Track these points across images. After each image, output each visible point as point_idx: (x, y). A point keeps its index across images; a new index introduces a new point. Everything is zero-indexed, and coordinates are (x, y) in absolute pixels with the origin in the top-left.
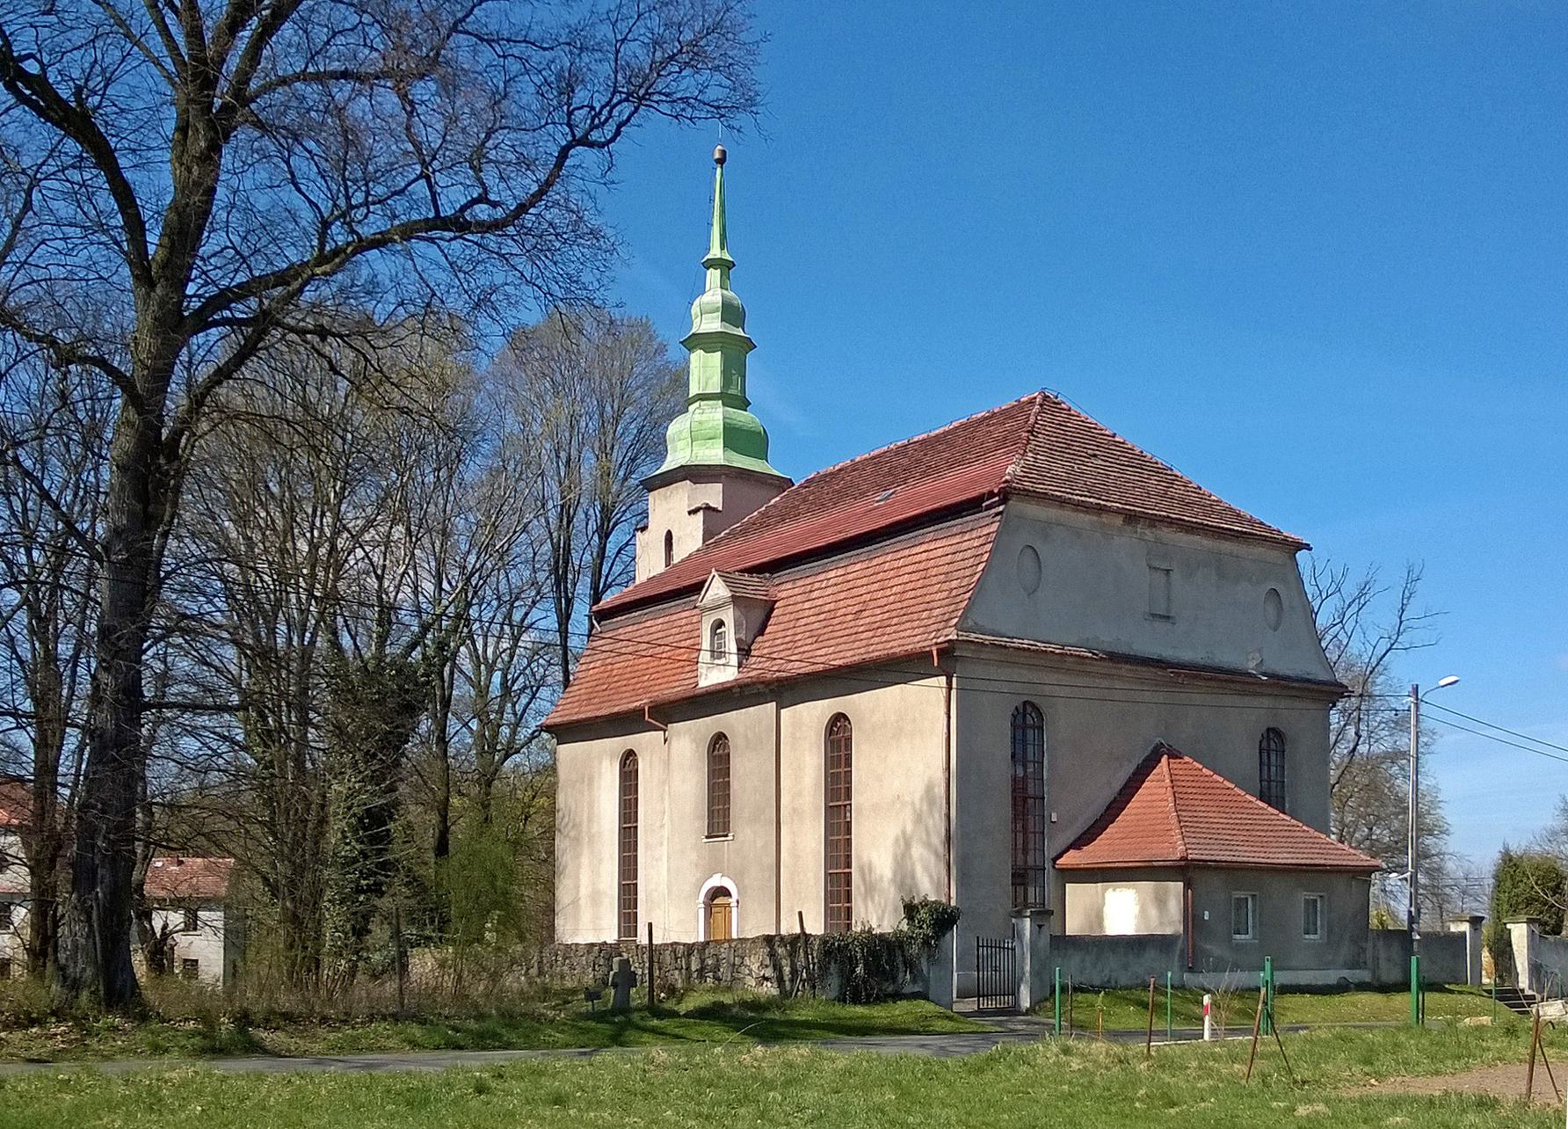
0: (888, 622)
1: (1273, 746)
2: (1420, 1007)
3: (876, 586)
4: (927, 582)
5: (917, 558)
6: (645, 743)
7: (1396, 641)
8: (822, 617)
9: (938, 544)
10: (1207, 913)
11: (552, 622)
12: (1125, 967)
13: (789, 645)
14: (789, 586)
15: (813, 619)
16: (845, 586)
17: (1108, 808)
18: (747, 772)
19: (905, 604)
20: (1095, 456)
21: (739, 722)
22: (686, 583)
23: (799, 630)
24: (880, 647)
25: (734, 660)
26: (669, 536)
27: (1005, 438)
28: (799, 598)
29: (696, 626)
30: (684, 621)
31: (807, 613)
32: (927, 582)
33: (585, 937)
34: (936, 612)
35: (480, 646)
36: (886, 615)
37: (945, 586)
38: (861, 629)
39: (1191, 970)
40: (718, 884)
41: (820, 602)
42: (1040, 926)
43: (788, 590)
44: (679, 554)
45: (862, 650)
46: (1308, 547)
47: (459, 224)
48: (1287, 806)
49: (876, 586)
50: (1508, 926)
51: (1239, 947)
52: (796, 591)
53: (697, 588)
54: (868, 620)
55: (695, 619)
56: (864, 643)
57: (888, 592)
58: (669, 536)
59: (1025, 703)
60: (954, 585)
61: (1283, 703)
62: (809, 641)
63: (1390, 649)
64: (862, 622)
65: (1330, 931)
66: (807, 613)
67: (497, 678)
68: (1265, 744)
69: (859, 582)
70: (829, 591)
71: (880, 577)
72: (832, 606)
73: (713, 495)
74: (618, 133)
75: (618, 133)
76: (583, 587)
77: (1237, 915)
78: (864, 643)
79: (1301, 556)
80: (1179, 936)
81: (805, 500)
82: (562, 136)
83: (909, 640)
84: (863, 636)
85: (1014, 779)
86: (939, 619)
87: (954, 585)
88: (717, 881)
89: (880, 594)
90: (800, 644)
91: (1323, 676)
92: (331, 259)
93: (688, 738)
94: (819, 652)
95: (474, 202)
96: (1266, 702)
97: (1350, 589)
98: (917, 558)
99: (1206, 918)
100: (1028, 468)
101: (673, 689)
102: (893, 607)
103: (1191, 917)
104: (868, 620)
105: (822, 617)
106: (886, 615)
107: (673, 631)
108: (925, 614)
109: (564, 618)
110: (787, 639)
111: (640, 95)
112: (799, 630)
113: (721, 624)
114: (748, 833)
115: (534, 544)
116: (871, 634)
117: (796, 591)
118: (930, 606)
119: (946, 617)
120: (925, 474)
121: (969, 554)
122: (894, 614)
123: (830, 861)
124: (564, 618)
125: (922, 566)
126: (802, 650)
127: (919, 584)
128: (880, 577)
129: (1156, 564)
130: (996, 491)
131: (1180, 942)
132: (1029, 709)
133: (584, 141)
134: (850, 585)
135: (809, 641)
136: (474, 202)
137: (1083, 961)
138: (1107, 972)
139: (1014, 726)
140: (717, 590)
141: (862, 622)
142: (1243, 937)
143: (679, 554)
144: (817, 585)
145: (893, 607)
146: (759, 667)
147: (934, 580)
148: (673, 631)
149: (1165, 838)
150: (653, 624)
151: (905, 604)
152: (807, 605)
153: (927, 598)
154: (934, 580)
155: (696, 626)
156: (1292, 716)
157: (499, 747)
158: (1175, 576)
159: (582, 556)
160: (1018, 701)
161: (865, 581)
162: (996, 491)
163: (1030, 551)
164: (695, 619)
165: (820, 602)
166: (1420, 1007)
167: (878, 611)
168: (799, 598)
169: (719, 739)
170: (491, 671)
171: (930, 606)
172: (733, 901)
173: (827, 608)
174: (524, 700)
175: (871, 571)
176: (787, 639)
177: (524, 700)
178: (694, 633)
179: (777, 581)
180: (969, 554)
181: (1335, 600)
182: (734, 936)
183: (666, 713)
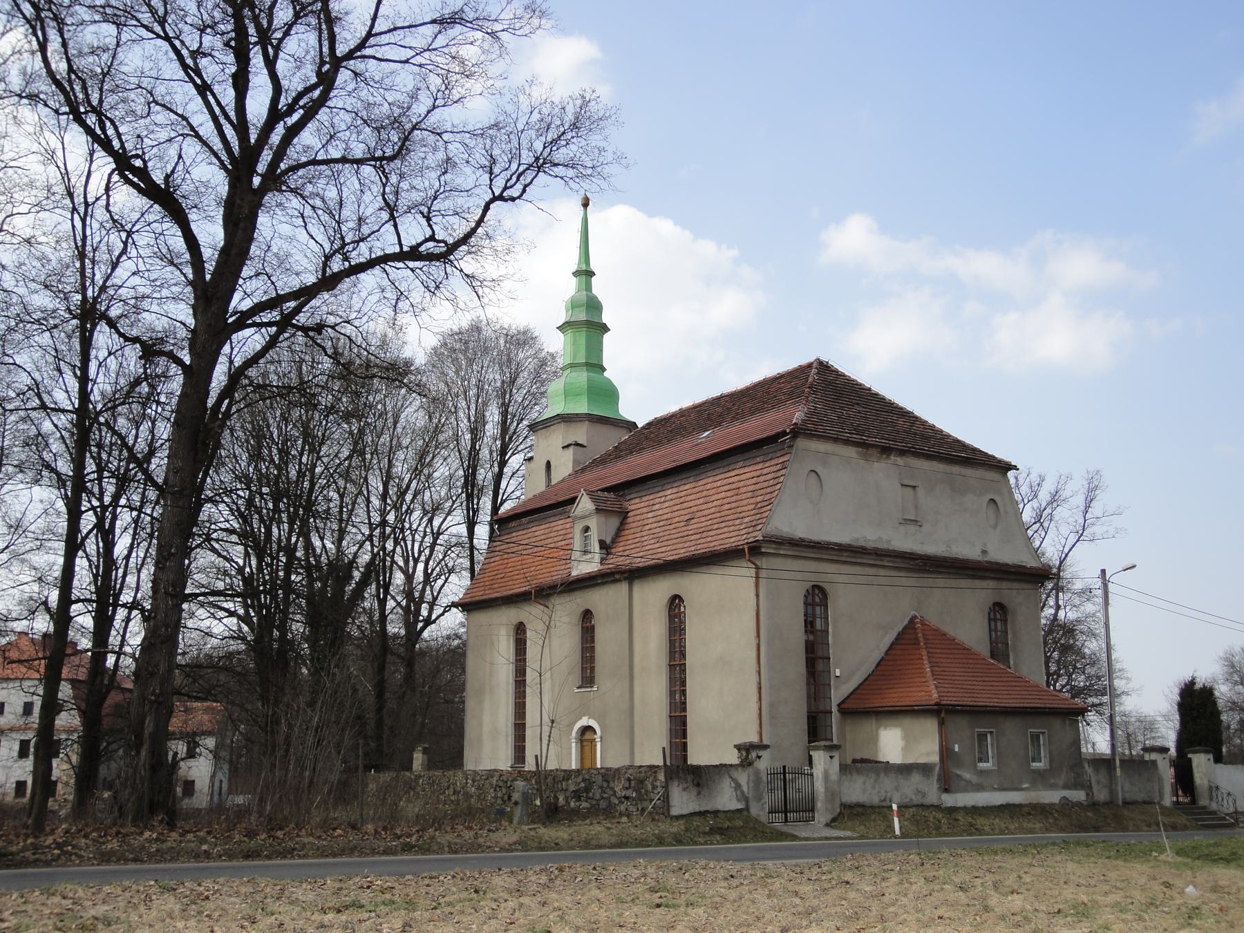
0: (710, 528)
1: (998, 616)
2: (217, 110)
3: (701, 501)
4: (739, 497)
5: (731, 480)
6: (532, 614)
7: (1082, 535)
8: (661, 524)
9: (746, 470)
10: (957, 746)
11: (463, 530)
12: (897, 789)
13: (638, 545)
14: (637, 501)
15: (655, 525)
16: (678, 501)
17: (878, 665)
18: (607, 638)
19: (723, 514)
20: (858, 404)
21: (604, 600)
22: (562, 499)
23: (644, 533)
24: (705, 545)
25: (597, 557)
26: (548, 464)
27: (792, 392)
28: (644, 510)
29: (569, 531)
30: (560, 527)
31: (650, 521)
32: (739, 497)
33: (486, 765)
34: (746, 520)
35: (409, 544)
36: (709, 523)
37: (752, 501)
38: (691, 532)
39: (946, 790)
40: (586, 724)
41: (660, 512)
42: (831, 757)
43: (639, 505)
44: (557, 477)
45: (693, 548)
46: (1015, 468)
47: (413, 254)
48: (1012, 662)
49: (701, 501)
50: (1190, 756)
51: (982, 773)
52: (642, 505)
53: (572, 501)
54: (695, 526)
55: (568, 526)
56: (693, 543)
57: (710, 505)
58: (548, 464)
59: (814, 586)
60: (759, 499)
61: (1004, 584)
62: (652, 541)
63: (1078, 540)
64: (690, 527)
65: (1051, 762)
66: (650, 521)
67: (421, 566)
68: (992, 616)
69: (689, 498)
70: (666, 504)
71: (705, 493)
72: (669, 516)
73: (580, 433)
74: (524, 191)
75: (524, 191)
76: (486, 503)
77: (980, 746)
78: (693, 543)
79: (1011, 474)
80: (935, 765)
81: (646, 438)
82: (489, 196)
83: (727, 541)
84: (693, 538)
85: (807, 642)
86: (749, 525)
87: (759, 499)
88: (584, 721)
89: (704, 507)
90: (645, 543)
91: (1031, 563)
92: (328, 282)
93: (565, 611)
94: (660, 550)
95: (426, 240)
96: (991, 584)
97: (1044, 496)
98: (731, 480)
99: (957, 750)
100: (810, 414)
101: (555, 575)
102: (713, 516)
103: (946, 753)
104: (695, 526)
105: (661, 524)
106: (709, 523)
107: (552, 535)
108: (738, 522)
109: (471, 525)
110: (636, 540)
111: (540, 165)
112: (644, 533)
113: (587, 529)
114: (606, 682)
115: (446, 468)
116: (698, 536)
117: (642, 505)
118: (742, 515)
119: (754, 523)
120: (734, 419)
121: (770, 476)
122: (716, 521)
123: (672, 704)
124: (471, 525)
125: (734, 486)
126: (647, 548)
127: (734, 499)
128: (705, 493)
129: (906, 482)
130: (788, 431)
131: (937, 768)
132: (817, 591)
133: (501, 198)
134: (682, 500)
135: (652, 541)
136: (426, 240)
137: (864, 783)
138: (883, 793)
139: (806, 604)
140: (585, 504)
141: (690, 527)
142: (985, 764)
143: (557, 477)
144: (657, 500)
145: (713, 516)
146: (615, 561)
147: (744, 496)
148: (552, 535)
149: (923, 689)
150: (539, 532)
151: (723, 514)
152: (650, 515)
153: (739, 510)
154: (744, 496)
155: (569, 531)
156: (1014, 595)
157: (421, 618)
158: (920, 491)
159: (484, 475)
160: (808, 585)
161: (693, 497)
162: (788, 431)
163: (813, 474)
164: (568, 526)
165: (660, 512)
166: (217, 110)
167: (703, 519)
168: (644, 510)
169: (587, 615)
170: (416, 561)
171: (742, 515)
172: (597, 737)
173: (665, 517)
174: (440, 582)
175: (697, 490)
176: (636, 540)
177: (440, 582)
178: (568, 536)
179: (628, 498)
180: (770, 476)
181: (1035, 504)
182: (599, 766)
183: (543, 593)
